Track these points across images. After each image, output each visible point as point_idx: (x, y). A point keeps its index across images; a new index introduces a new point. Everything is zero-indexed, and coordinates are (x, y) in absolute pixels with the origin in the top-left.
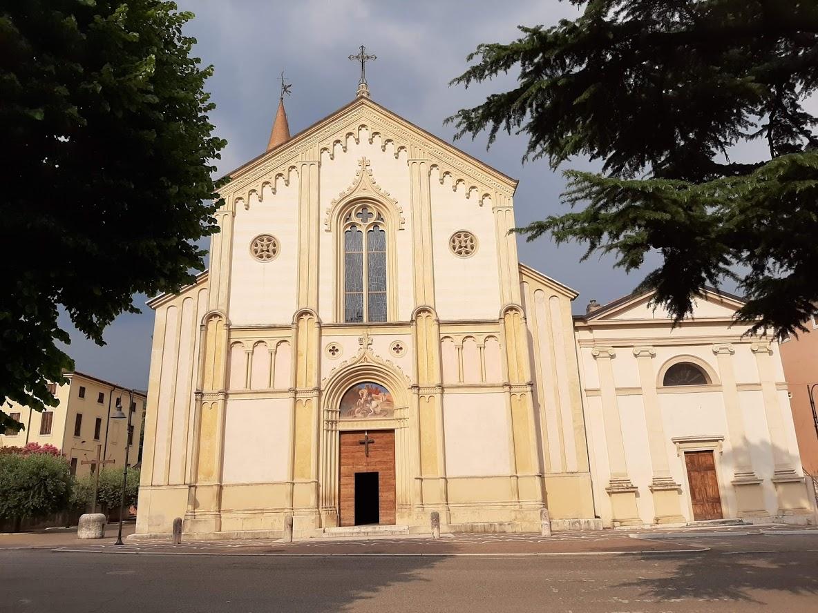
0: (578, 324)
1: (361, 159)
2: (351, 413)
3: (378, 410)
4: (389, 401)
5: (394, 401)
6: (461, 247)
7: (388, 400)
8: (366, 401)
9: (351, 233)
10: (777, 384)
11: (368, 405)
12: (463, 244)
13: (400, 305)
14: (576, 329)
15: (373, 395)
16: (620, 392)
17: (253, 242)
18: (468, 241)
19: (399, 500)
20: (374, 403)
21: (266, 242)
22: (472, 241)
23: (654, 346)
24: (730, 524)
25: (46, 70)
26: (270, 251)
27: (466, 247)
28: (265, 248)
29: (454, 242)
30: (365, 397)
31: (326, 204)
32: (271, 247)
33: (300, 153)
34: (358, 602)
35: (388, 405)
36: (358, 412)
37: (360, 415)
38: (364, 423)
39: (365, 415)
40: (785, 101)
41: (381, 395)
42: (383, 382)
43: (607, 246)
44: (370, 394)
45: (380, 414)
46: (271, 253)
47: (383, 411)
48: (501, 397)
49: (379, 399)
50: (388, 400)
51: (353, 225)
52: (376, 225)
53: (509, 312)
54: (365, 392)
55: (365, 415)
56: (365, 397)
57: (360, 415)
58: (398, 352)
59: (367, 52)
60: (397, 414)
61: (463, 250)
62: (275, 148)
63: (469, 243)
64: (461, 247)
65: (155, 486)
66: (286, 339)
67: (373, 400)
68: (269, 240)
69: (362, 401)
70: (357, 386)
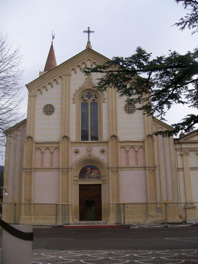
0: (176, 142)
1: (84, 73)
2: (84, 178)
3: (95, 176)
4: (99, 173)
5: (101, 173)
6: (129, 110)
8: (90, 173)
9: (84, 105)
10: (190, 168)
14: (175, 143)
15: (93, 171)
16: (191, 169)
17: (47, 105)
18: (132, 107)
20: (93, 174)
21: (49, 107)
22: (53, 109)
23: (189, 151)
24: (171, 224)
26: (51, 111)
27: (131, 110)
28: (49, 110)
29: (45, 109)
31: (73, 91)
32: (51, 110)
33: (63, 71)
35: (98, 174)
36: (86, 177)
37: (87, 178)
38: (89, 181)
39: (89, 178)
41: (95, 171)
42: (94, 164)
44: (91, 170)
45: (95, 178)
46: (46, 112)
47: (97, 177)
48: (141, 172)
49: (95, 172)
51: (84, 100)
52: (94, 100)
53: (29, 139)
54: (89, 169)
55: (89, 178)
56: (89, 171)
57: (87, 178)
58: (103, 153)
59: (91, 30)
60: (102, 178)
61: (130, 111)
62: (54, 68)
63: (51, 110)
64: (48, 111)
65: (109, 204)
66: (48, 147)
68: (50, 107)
69: (88, 173)
70: (89, 167)
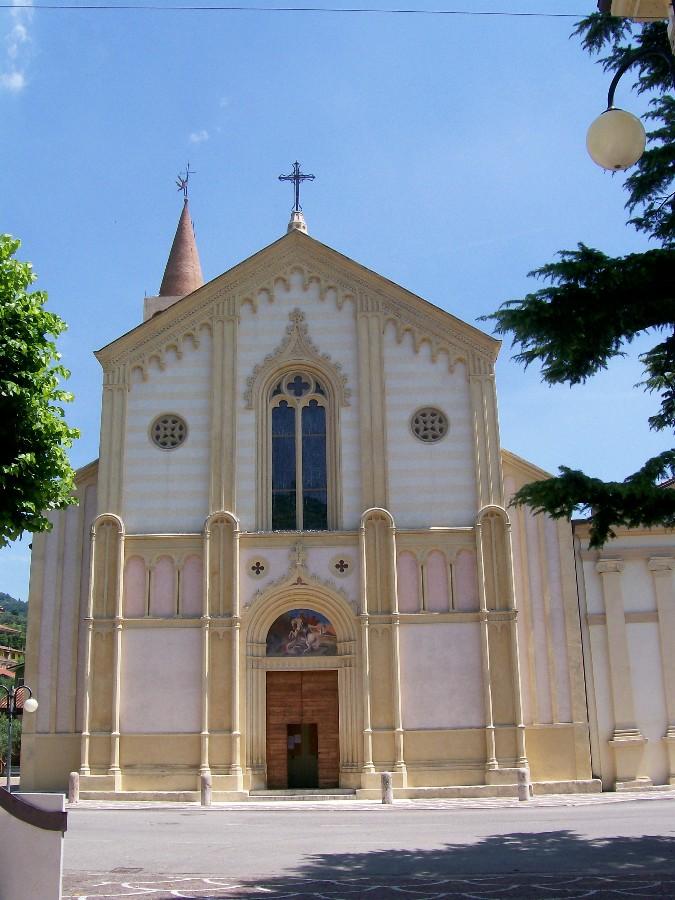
3: (317, 645)
4: (331, 634)
7: (328, 633)
8: (301, 634)
11: (302, 639)
12: (429, 425)
13: (346, 497)
15: (310, 626)
18: (422, 429)
19: (343, 759)
20: (311, 637)
25: (10, 343)
30: (298, 628)
31: (244, 371)
34: (296, 865)
36: (291, 648)
40: (293, 622)
41: (320, 625)
42: (223, 350)
43: (647, 382)
44: (305, 625)
50: (328, 633)
54: (299, 622)
56: (298, 628)
59: (303, 171)
67: (308, 632)
69: (296, 633)
